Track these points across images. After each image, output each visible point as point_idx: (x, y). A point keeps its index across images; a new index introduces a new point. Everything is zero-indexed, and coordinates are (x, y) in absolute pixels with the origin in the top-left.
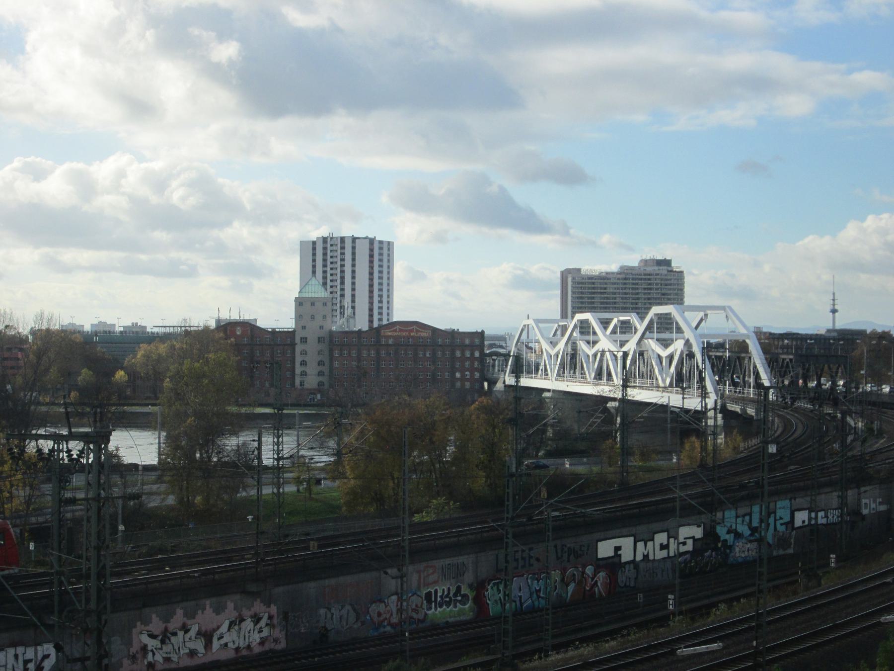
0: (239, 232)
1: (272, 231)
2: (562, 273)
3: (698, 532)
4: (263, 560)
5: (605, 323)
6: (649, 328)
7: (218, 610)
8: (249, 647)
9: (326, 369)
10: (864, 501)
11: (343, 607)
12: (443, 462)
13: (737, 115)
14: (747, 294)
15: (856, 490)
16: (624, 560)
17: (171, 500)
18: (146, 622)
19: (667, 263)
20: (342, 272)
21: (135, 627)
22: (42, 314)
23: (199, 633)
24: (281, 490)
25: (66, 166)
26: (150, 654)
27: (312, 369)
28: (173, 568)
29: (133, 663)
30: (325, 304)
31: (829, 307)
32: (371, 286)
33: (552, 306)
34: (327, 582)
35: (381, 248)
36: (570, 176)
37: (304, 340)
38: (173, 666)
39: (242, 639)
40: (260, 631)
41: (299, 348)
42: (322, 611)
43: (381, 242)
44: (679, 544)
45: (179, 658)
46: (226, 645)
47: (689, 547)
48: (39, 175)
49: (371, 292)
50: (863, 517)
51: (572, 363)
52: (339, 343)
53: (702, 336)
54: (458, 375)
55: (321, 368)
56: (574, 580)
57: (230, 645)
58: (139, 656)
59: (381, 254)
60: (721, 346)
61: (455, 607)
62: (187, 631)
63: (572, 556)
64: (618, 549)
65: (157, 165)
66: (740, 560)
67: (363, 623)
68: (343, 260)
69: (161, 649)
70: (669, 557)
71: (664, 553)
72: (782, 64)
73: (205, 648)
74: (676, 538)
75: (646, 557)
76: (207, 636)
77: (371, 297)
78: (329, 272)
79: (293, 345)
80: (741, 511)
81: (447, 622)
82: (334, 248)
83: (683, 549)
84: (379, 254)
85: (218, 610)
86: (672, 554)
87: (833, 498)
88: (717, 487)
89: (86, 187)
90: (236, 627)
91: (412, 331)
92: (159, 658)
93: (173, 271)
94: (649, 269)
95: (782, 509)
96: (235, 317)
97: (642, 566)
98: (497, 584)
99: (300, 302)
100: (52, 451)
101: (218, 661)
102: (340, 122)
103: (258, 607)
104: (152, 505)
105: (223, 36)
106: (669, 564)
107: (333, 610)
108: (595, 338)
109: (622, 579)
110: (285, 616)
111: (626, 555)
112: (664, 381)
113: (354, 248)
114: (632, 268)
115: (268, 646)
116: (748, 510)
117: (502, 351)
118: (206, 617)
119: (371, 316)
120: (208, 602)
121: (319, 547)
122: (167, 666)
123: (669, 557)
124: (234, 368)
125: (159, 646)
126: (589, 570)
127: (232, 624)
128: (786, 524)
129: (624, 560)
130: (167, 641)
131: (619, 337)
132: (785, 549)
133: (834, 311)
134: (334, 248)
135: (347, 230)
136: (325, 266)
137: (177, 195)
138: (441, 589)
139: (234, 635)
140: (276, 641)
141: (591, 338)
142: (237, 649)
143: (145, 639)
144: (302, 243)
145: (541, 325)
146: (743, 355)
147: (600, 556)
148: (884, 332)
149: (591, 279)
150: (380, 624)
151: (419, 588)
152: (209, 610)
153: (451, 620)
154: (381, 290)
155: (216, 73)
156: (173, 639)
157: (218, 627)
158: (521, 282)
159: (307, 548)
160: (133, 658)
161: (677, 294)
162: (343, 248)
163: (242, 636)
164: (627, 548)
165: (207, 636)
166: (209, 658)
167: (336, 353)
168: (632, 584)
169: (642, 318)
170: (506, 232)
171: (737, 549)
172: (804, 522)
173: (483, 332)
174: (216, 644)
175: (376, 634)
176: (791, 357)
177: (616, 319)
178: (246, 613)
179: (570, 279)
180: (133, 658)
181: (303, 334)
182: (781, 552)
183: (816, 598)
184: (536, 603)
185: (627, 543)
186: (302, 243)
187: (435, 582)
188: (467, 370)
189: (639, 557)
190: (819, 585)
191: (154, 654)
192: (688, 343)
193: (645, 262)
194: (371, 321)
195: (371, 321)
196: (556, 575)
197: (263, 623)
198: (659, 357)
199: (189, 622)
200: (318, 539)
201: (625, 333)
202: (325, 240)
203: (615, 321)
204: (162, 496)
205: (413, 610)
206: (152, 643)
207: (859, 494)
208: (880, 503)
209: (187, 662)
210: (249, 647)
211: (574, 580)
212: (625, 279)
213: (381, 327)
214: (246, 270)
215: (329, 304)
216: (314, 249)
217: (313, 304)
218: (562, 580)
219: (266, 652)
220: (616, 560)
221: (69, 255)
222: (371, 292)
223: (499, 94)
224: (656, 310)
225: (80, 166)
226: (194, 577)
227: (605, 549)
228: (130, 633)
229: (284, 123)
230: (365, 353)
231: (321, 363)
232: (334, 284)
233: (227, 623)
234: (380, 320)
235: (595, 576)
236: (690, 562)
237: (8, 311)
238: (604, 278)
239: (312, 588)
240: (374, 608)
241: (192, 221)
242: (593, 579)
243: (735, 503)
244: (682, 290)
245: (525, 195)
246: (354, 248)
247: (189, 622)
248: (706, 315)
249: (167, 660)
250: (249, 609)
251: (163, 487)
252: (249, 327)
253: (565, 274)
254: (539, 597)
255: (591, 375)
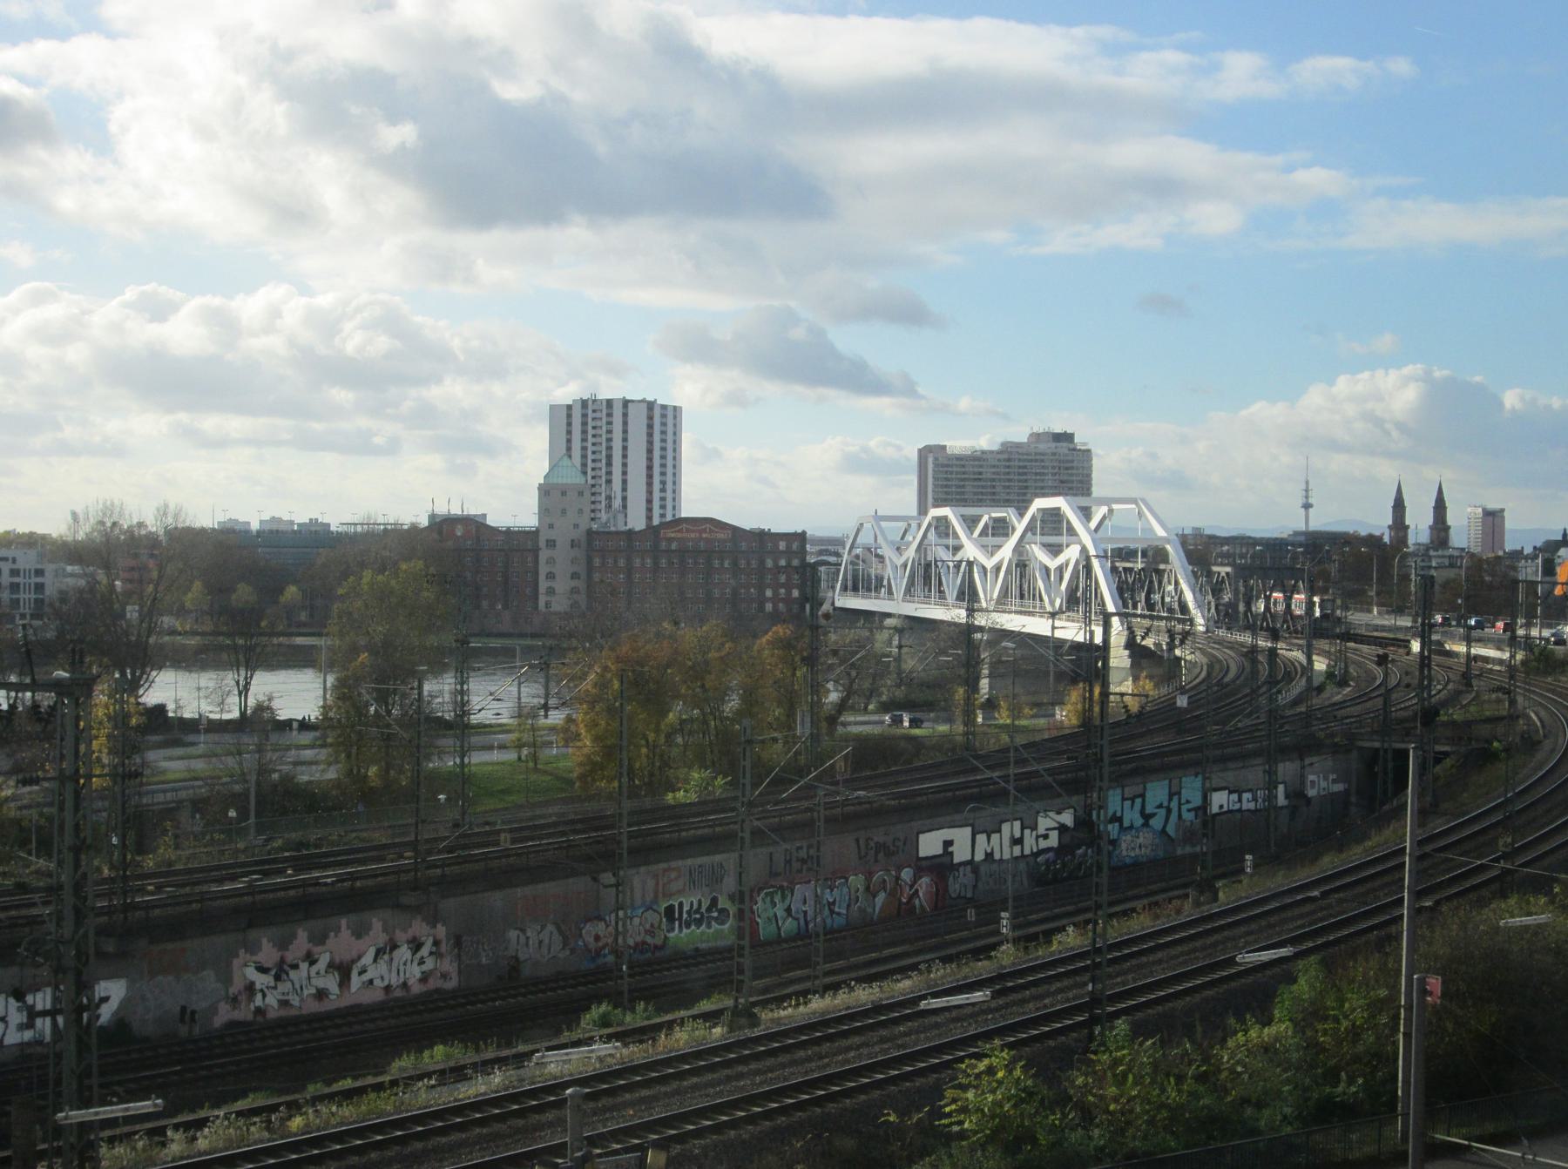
0: (453, 391)
1: (498, 389)
2: (920, 451)
3: (1067, 818)
4: (424, 860)
5: (971, 522)
6: (1030, 528)
7: (359, 932)
8: (405, 985)
9: (580, 584)
10: (1311, 777)
11: (543, 927)
12: (722, 719)
13: (1136, 232)
14: (1177, 481)
15: (1297, 764)
16: (956, 860)
17: (332, 774)
18: (253, 949)
19: (1067, 437)
20: (609, 448)
21: (237, 956)
22: (166, 506)
23: (331, 966)
24: (466, 760)
25: (197, 301)
26: (259, 996)
27: (562, 585)
28: (298, 870)
29: (234, 1008)
30: (581, 494)
31: (1301, 501)
32: (650, 468)
33: (904, 497)
34: (519, 891)
35: (664, 416)
36: (909, 314)
37: (551, 544)
38: (294, 1012)
39: (394, 974)
40: (422, 962)
41: (544, 555)
42: (513, 934)
43: (664, 407)
44: (1038, 837)
45: (302, 1000)
46: (371, 982)
47: (1054, 840)
48: (159, 311)
49: (650, 477)
50: (1309, 801)
51: (926, 577)
52: (602, 547)
53: (1102, 540)
54: (769, 593)
55: (575, 583)
56: (884, 889)
57: (377, 982)
58: (243, 998)
59: (664, 424)
60: (1129, 554)
61: (709, 926)
62: (313, 963)
63: (881, 855)
64: (948, 844)
65: (325, 300)
66: (1128, 861)
67: (573, 951)
68: (609, 432)
69: (275, 988)
70: (1023, 856)
71: (1017, 850)
72: (1190, 156)
73: (340, 985)
74: (1034, 828)
75: (989, 856)
76: (343, 970)
77: (650, 484)
78: (590, 449)
79: (535, 551)
80: (1129, 792)
81: (697, 949)
82: (598, 415)
83: (1043, 844)
84: (661, 423)
85: (359, 932)
86: (1027, 851)
87: (1255, 774)
88: (1103, 755)
89: (225, 324)
90: (386, 957)
91: (704, 531)
92: (272, 1000)
93: (362, 446)
94: (1042, 447)
95: (1191, 789)
96: (456, 510)
97: (983, 869)
98: (771, 895)
99: (545, 491)
100: (52, 708)
101: (359, 1006)
102: (576, 234)
103: (419, 928)
104: (305, 778)
105: (394, 118)
106: (1022, 866)
107: (529, 934)
108: (956, 542)
109: (954, 887)
110: (458, 942)
111: (961, 853)
112: (1052, 603)
113: (625, 415)
114: (1018, 445)
115: (433, 984)
116: (1139, 789)
117: (832, 559)
118: (342, 942)
119: (650, 510)
120: (344, 922)
121: (514, 841)
122: (283, 1013)
123: (1023, 856)
124: (454, 581)
125: (272, 984)
126: (907, 874)
127: (379, 953)
128: (1196, 809)
129: (956, 860)
130: (284, 977)
131: (990, 540)
132: (1193, 845)
133: (1307, 506)
134: (598, 415)
135: (610, 389)
136: (584, 440)
137: (353, 341)
138: (689, 901)
139: (382, 967)
140: (444, 976)
141: (951, 542)
142: (388, 988)
143: (252, 974)
144: (552, 408)
145: (883, 524)
146: (1162, 567)
147: (922, 854)
148: (1371, 536)
149: (961, 459)
150: (598, 952)
151: (655, 900)
152: (345, 933)
153: (704, 946)
154: (663, 474)
155: (393, 164)
156: (293, 974)
157: (359, 957)
158: (858, 463)
159: (497, 844)
160: (234, 1001)
161: (1081, 482)
162: (609, 415)
163: (394, 969)
164: (962, 843)
165: (343, 970)
166: (346, 1002)
167: (597, 562)
168: (969, 895)
169: (1022, 515)
170: (831, 393)
171: (1124, 846)
172: (1221, 807)
173: (804, 533)
174: (356, 981)
175: (592, 966)
176: (1228, 569)
177: (987, 516)
178: (400, 936)
179: (930, 460)
180: (234, 1001)
181: (552, 535)
182: (1188, 849)
183: (1211, 917)
184: (829, 921)
185: (961, 836)
186: (552, 408)
187: (681, 892)
188: (783, 585)
189: (979, 856)
190: (1216, 899)
191: (264, 996)
192: (1084, 550)
193: (1036, 437)
194: (649, 518)
195: (649, 518)
196: (857, 881)
197: (424, 951)
198: (1047, 570)
199: (316, 950)
200: (511, 831)
201: (998, 535)
202: (584, 403)
203: (985, 518)
204: (322, 767)
205: (646, 932)
206: (262, 980)
207: (1303, 768)
208: (1334, 781)
209: (314, 1007)
210: (405, 985)
211: (884, 889)
212: (1009, 460)
213: (664, 525)
214: (467, 444)
215: (587, 494)
216: (569, 416)
217: (564, 493)
218: (867, 889)
219: (429, 993)
220: (946, 860)
221: (210, 423)
222: (650, 477)
223: (800, 197)
224: (1040, 503)
225: (217, 301)
226: (326, 884)
227: (929, 844)
228: (229, 965)
229: (497, 237)
230: (637, 562)
231: (575, 576)
232: (598, 465)
233: (372, 952)
234: (663, 516)
235: (915, 882)
236: (1054, 862)
237: (117, 502)
238: (979, 458)
239: (497, 899)
240: (590, 930)
241: (389, 379)
242: (911, 887)
243: (1119, 779)
244: (1089, 476)
245: (849, 340)
246: (625, 415)
247: (316, 950)
248: (1111, 511)
249: (284, 1003)
250: (404, 930)
251: (323, 754)
252: (475, 526)
253: (924, 452)
254: (832, 912)
255: (951, 595)
